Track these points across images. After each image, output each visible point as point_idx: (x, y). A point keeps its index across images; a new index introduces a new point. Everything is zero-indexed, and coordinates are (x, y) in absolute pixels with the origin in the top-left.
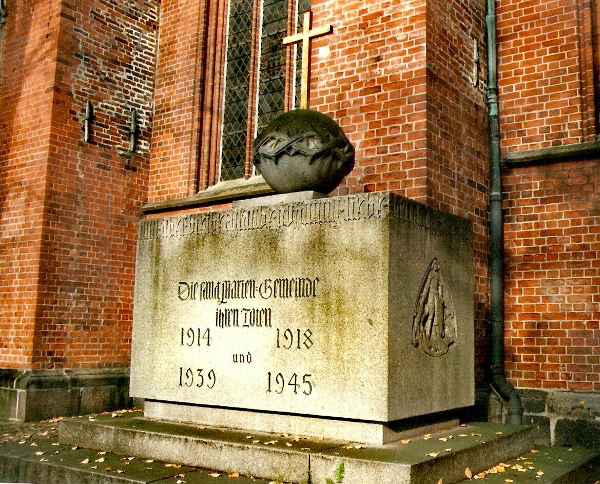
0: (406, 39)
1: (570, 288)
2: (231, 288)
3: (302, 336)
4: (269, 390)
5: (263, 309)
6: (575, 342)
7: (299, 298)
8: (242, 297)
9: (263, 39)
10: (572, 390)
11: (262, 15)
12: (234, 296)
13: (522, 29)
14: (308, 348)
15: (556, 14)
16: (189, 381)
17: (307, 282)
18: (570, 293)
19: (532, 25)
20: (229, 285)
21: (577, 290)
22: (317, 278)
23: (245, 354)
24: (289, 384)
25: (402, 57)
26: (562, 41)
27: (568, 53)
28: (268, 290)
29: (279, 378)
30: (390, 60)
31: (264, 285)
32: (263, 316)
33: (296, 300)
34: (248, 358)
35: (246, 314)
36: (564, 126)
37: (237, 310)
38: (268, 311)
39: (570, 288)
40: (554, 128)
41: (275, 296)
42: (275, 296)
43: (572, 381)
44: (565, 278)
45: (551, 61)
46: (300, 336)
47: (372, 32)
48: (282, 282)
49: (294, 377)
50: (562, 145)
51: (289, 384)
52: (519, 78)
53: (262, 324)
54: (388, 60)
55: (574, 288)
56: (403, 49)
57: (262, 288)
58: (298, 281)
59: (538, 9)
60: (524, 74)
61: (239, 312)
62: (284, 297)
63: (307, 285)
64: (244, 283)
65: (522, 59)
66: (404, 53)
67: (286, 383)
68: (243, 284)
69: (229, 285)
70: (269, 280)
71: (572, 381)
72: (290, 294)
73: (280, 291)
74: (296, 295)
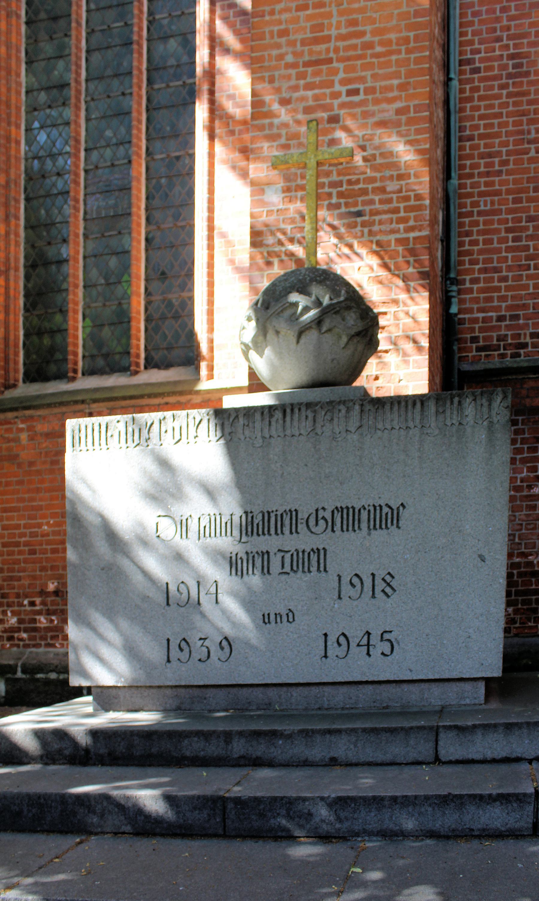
0: (400, 191)
1: (521, 525)
2: (256, 522)
3: (378, 581)
4: (326, 656)
5: (312, 550)
6: (524, 583)
7: (373, 532)
8: (276, 533)
9: (86, 171)
10: (516, 635)
11: (83, 133)
12: (260, 532)
13: (479, 206)
14: (388, 596)
15: (522, 193)
16: (184, 656)
17: (385, 510)
18: (521, 530)
19: (492, 203)
20: (252, 517)
21: (529, 527)
22: (402, 504)
23: (284, 612)
24: (358, 645)
25: (394, 216)
26: (527, 228)
27: (534, 245)
28: (322, 523)
29: (342, 640)
30: (377, 218)
31: (314, 515)
32: (314, 558)
33: (369, 534)
34: (291, 616)
35: (283, 557)
36: (525, 334)
37: (268, 552)
38: (322, 552)
39: (521, 525)
40: (514, 337)
41: (333, 531)
42: (333, 531)
43: (518, 625)
44: (517, 514)
45: (514, 252)
46: (376, 582)
47: (349, 174)
48: (345, 511)
49: (366, 637)
50: (522, 358)
51: (358, 645)
52: (474, 269)
53: (311, 569)
54: (373, 218)
55: (527, 524)
56: (395, 204)
57: (310, 520)
58: (372, 509)
59: (501, 183)
60: (481, 266)
61: (271, 554)
62: (348, 530)
63: (387, 514)
64: (279, 513)
65: (478, 245)
66: (396, 211)
67: (353, 645)
68: (276, 515)
69: (252, 517)
70: (323, 509)
71: (518, 625)
72: (359, 527)
73: (342, 522)
74: (369, 527)
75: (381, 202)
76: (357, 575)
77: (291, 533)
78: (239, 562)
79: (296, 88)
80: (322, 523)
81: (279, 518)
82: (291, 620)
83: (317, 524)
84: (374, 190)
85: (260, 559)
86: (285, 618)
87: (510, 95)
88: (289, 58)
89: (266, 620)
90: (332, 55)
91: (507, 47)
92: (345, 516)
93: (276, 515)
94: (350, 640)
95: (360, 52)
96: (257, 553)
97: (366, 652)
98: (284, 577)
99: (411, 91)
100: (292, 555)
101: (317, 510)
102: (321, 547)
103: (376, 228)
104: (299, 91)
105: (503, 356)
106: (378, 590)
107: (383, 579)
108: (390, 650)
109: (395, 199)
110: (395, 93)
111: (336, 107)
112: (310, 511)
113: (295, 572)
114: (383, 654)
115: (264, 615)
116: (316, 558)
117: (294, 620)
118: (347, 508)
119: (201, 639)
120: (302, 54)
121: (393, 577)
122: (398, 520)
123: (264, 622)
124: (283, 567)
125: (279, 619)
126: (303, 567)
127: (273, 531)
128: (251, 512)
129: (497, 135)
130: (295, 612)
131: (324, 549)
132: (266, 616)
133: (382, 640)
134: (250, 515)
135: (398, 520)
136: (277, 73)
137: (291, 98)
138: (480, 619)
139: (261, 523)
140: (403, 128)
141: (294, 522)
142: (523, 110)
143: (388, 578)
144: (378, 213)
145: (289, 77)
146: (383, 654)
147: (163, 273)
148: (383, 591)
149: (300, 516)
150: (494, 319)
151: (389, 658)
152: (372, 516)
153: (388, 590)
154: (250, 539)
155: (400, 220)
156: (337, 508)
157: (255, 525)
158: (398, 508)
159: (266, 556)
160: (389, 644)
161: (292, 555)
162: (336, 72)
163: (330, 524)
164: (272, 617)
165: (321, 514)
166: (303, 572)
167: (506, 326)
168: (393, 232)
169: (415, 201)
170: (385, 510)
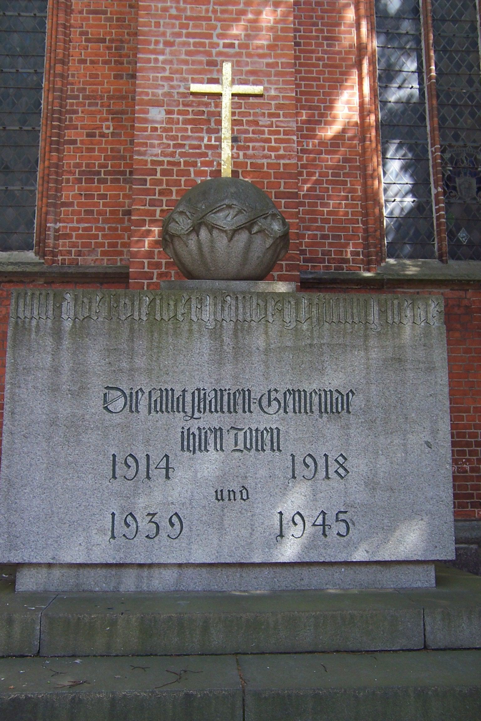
17: (335, 395)
23: (237, 490)
24: (314, 525)
28: (274, 403)
33: (321, 417)
36: (346, 252)
41: (286, 412)
42: (286, 412)
50: (345, 271)
51: (314, 525)
63: (337, 399)
64: (232, 392)
68: (229, 394)
69: (205, 394)
70: (276, 390)
75: (253, 133)
76: (310, 455)
77: (244, 412)
78: (191, 437)
79: (179, 35)
80: (274, 403)
81: (232, 397)
82: (245, 497)
83: (269, 405)
84: (248, 122)
85: (213, 435)
86: (238, 495)
87: (325, 66)
88: (174, 12)
89: (219, 497)
90: (210, 14)
91: (322, 31)
92: (297, 399)
93: (229, 394)
94: (305, 519)
95: (234, 16)
96: (210, 429)
97: (321, 532)
98: (237, 454)
99: (279, 52)
100: (245, 433)
101: (269, 392)
102: (274, 427)
103: (250, 152)
104: (182, 38)
105: (327, 268)
106: (331, 471)
107: (336, 460)
108: (345, 530)
109: (266, 132)
110: (266, 51)
111: (214, 54)
112: (264, 392)
113: (249, 450)
114: (338, 534)
115: (216, 492)
116: (269, 437)
117: (248, 498)
118: (299, 391)
119: (149, 514)
120: (185, 10)
121: (345, 459)
122: (150, 404)
123: (217, 499)
124: (236, 444)
125: (232, 496)
126: (257, 445)
127: (225, 409)
128: (204, 389)
129: (317, 94)
130: (249, 489)
131: (277, 428)
132: (219, 493)
133: (337, 520)
134: (202, 392)
135: (150, 404)
136: (162, 22)
137: (174, 41)
138: (431, 502)
139: (213, 400)
140: (273, 78)
141: (247, 401)
142: (337, 78)
143: (341, 460)
144: (251, 140)
145: (173, 26)
146: (338, 534)
147: (7, 167)
148: (336, 472)
149: (252, 395)
150: (319, 236)
151: (345, 538)
152: (323, 400)
153: (341, 471)
154: (201, 415)
155: (271, 149)
156: (288, 390)
157: (207, 402)
158: (348, 394)
159: (219, 433)
160: (344, 524)
161: (245, 433)
162: (215, 28)
163: (282, 405)
164: (225, 493)
165: (273, 395)
166: (257, 450)
167: (329, 243)
168: (266, 157)
169: (284, 135)
170: (335, 395)
